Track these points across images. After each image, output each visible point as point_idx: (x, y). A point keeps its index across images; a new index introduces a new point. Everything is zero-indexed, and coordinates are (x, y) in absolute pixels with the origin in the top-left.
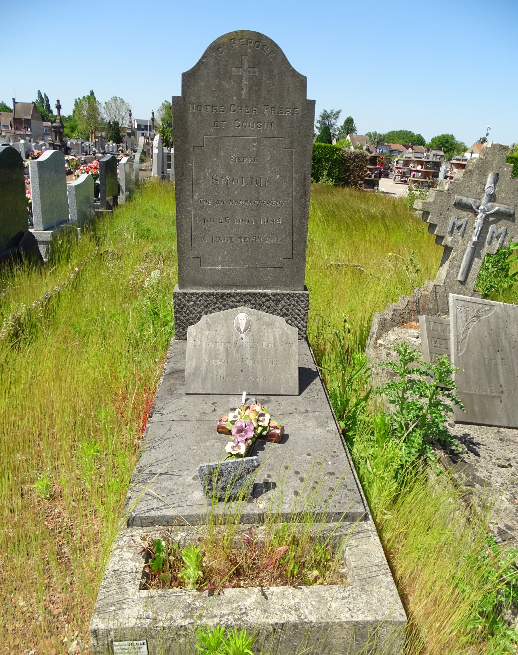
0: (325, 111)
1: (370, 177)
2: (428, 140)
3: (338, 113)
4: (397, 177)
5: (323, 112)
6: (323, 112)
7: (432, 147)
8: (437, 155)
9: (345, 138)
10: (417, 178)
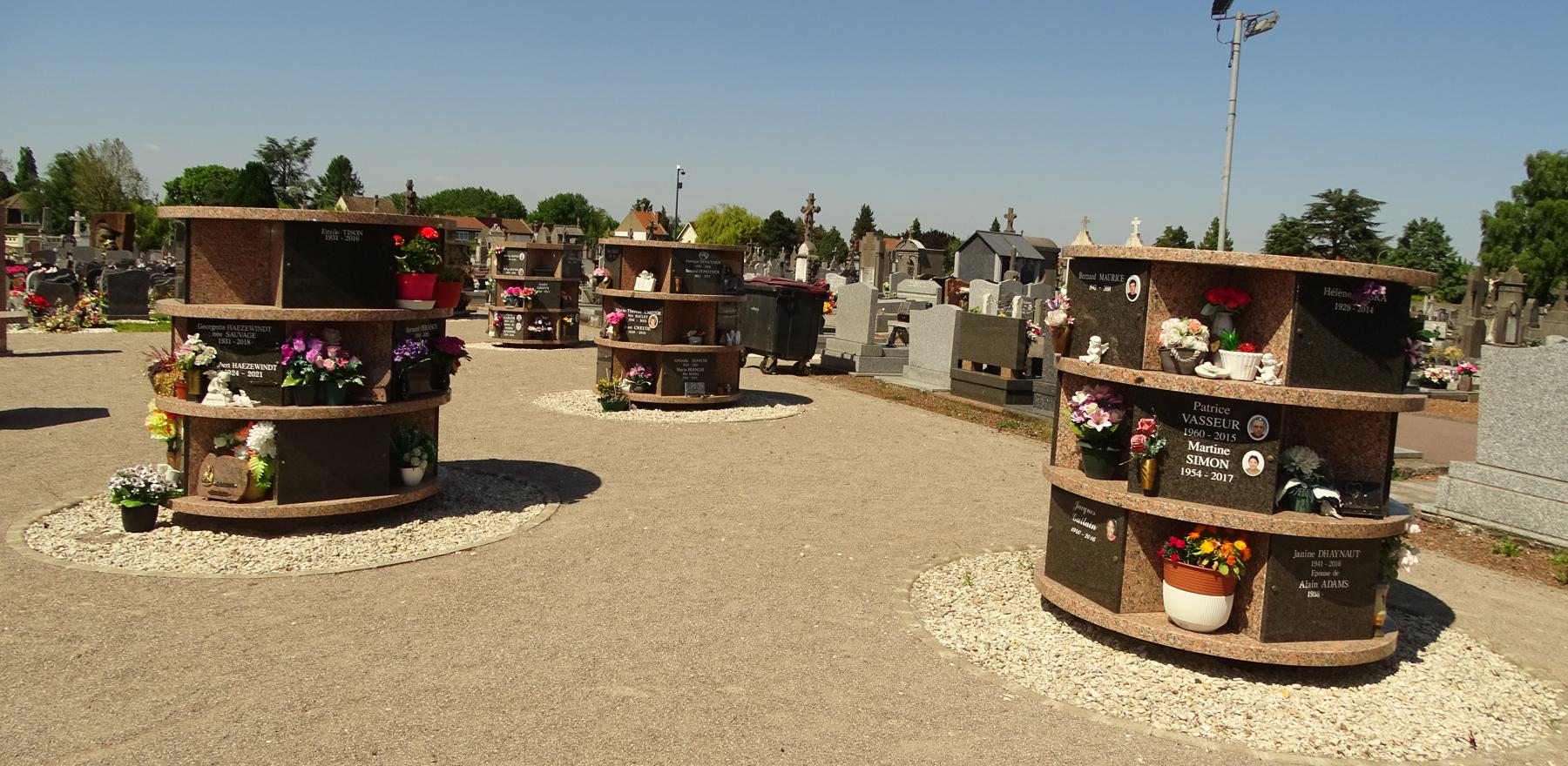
0: (272, 141)
1: (353, 395)
2: (531, 207)
3: (308, 145)
4: (507, 318)
5: (266, 143)
6: (266, 143)
7: (541, 220)
8: (568, 237)
9: (333, 205)
10: (638, 338)
